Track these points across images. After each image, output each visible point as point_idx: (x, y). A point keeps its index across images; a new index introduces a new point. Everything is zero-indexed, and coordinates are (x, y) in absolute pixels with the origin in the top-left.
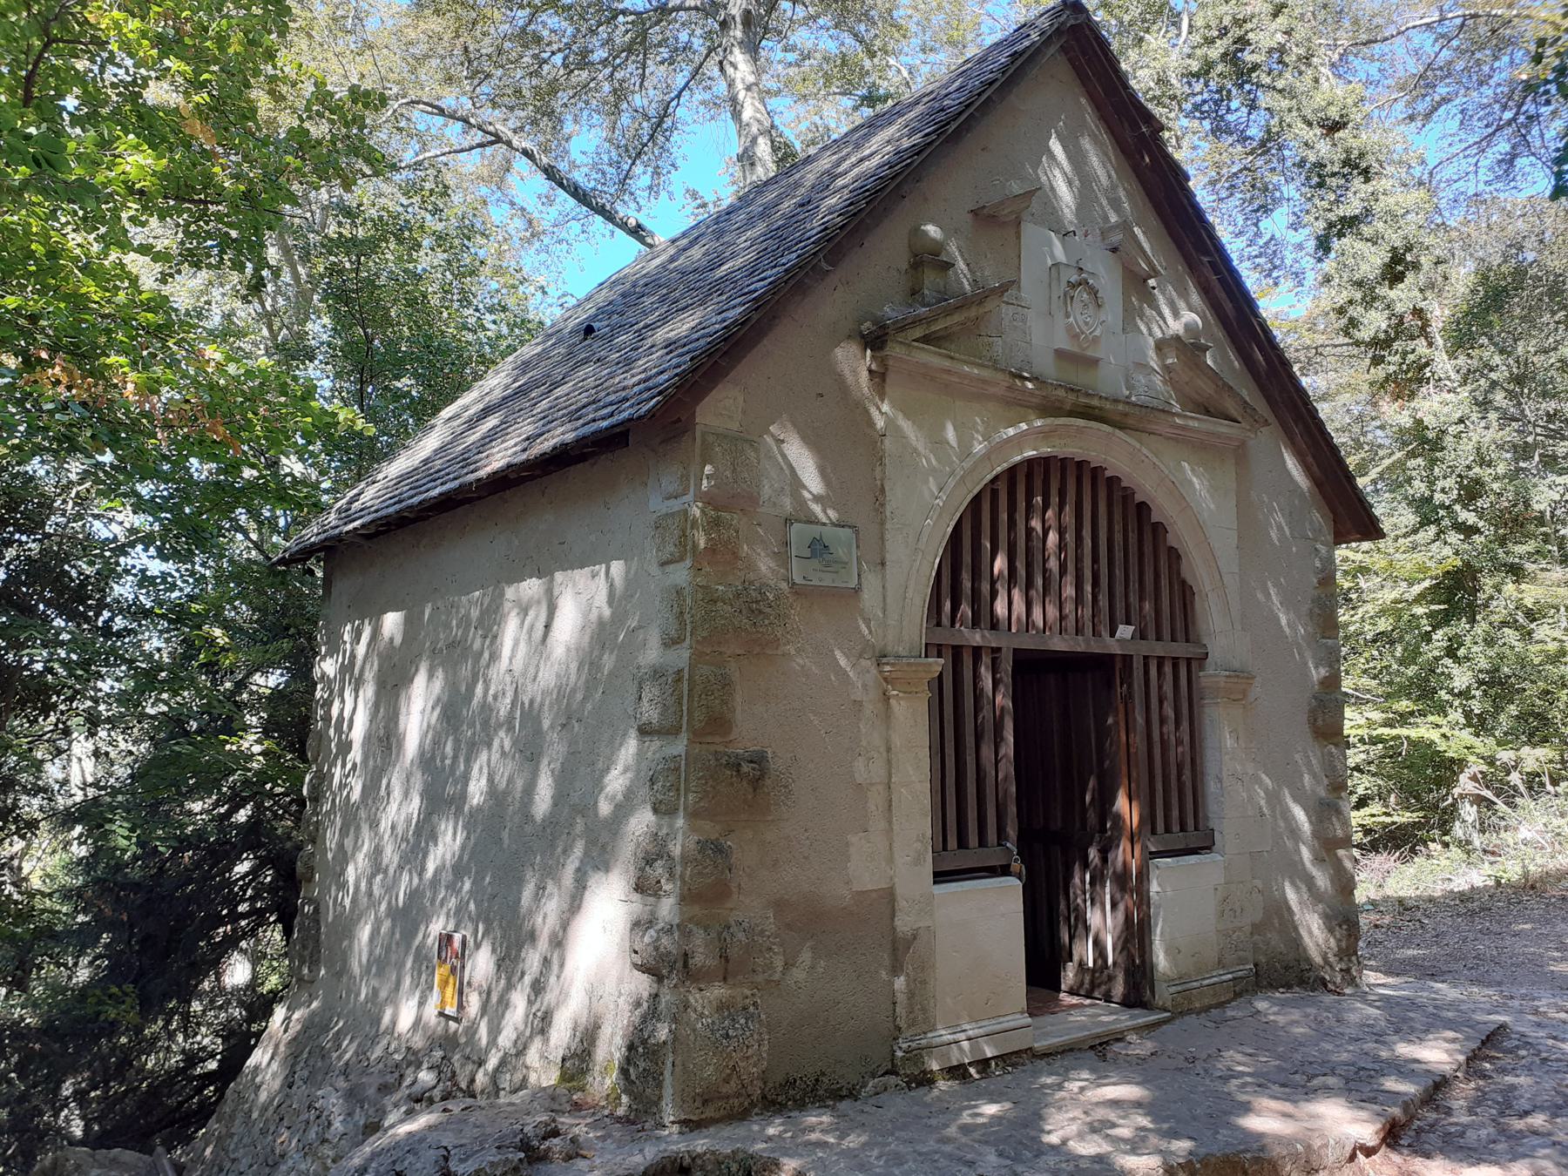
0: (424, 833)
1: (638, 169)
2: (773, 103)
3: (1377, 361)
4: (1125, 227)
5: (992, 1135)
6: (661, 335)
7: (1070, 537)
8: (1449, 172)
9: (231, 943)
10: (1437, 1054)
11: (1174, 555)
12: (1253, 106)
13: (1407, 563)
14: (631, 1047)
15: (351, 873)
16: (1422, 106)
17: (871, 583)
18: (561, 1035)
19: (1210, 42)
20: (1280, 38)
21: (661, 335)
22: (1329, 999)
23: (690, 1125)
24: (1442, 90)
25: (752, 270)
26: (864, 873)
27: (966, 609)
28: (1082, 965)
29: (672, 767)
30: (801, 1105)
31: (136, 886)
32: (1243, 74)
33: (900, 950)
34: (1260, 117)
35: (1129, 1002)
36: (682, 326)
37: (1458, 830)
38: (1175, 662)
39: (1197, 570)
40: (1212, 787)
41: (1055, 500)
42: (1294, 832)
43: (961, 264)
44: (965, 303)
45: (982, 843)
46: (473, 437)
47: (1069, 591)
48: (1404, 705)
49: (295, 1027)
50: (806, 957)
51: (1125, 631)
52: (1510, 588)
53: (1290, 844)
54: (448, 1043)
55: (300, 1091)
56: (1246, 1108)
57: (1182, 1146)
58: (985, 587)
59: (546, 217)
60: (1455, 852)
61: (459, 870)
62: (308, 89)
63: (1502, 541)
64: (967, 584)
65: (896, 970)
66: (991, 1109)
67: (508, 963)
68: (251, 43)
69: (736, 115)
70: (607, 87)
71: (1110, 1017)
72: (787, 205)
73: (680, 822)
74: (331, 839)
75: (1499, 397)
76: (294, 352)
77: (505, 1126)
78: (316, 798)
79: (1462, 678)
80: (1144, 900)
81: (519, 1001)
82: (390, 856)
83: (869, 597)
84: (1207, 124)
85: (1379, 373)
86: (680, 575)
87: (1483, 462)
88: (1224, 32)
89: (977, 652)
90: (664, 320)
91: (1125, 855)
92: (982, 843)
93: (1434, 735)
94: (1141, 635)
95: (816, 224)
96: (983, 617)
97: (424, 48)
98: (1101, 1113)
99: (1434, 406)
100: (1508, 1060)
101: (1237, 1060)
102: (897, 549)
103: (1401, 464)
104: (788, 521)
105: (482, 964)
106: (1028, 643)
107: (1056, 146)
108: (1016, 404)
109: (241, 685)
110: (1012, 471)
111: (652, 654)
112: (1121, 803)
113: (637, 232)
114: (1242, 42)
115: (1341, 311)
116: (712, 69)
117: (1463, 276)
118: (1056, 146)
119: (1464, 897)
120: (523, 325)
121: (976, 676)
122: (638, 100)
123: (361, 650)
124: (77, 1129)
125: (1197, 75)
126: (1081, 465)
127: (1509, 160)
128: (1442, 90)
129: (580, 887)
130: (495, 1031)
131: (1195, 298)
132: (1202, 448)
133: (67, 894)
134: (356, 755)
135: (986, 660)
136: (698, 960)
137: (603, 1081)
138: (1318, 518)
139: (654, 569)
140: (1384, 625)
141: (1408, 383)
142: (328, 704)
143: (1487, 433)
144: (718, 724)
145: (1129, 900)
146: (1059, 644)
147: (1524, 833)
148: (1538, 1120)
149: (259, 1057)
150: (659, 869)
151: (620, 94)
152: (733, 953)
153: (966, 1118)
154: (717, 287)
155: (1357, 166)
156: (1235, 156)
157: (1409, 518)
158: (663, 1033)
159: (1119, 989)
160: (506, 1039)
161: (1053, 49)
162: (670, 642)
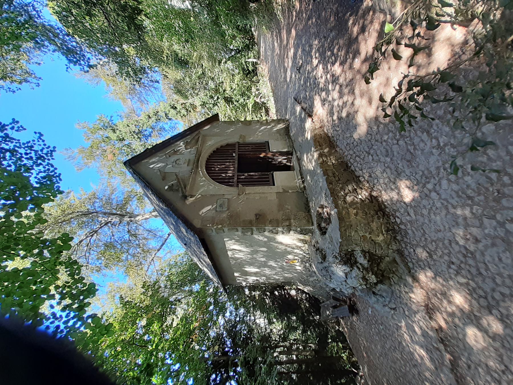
0: (271, 267)
1: (158, 234)
2: (146, 211)
3: (190, 111)
4: (165, 155)
5: (312, 178)
6: (185, 234)
7: (219, 164)
8: (157, 98)
9: (289, 294)
10: (298, 109)
11: (222, 147)
12: (146, 130)
13: (223, 108)
14: (301, 234)
15: (277, 278)
16: (146, 102)
17: (226, 197)
18: (300, 244)
19: (134, 137)
20: (133, 125)
21: (185, 234)
22: (291, 124)
23: (313, 224)
24: (143, 99)
25: (174, 219)
26: (274, 197)
27: (231, 180)
28: (287, 162)
29: (258, 229)
30: (309, 206)
31: (280, 311)
32: (140, 132)
33: (285, 191)
34: (148, 129)
35: (292, 155)
36: (183, 230)
37: (266, 102)
38: (239, 147)
39: (224, 143)
40: (258, 141)
41: (213, 166)
42: (265, 129)
43: (172, 183)
44: (179, 181)
45: (268, 178)
46: (204, 263)
47: (228, 164)
48: (246, 109)
49: (301, 285)
50: (287, 206)
51: (234, 155)
52: (227, 92)
53: (266, 130)
54: (302, 261)
55: (310, 283)
56: (307, 138)
57: (313, 149)
58: (227, 177)
59: (167, 250)
60: (269, 102)
61: (276, 261)
62: (142, 296)
63: (220, 93)
64: (226, 180)
65: (288, 192)
66: (308, 177)
67: (290, 253)
68: (133, 308)
69: (148, 218)
70: (143, 241)
71: (294, 159)
72: (162, 212)
73: (266, 228)
74: (272, 281)
75: (196, 92)
76: (191, 292)
77: (314, 253)
78: (265, 284)
79: (242, 100)
80: (276, 152)
81: (295, 251)
82: (274, 272)
83: (229, 197)
84: (149, 138)
85: (192, 111)
86: (226, 229)
87: (207, 95)
88: (132, 135)
89: (238, 179)
90: (182, 233)
91: (270, 155)
92: (268, 178)
93: (251, 105)
94: (234, 152)
95: (165, 208)
96: (232, 178)
97: (136, 274)
98: (308, 160)
99: (198, 102)
100: (299, 97)
101: (300, 139)
102: (222, 192)
103: (208, 108)
104: (216, 211)
105: (290, 257)
106: (236, 170)
107: (151, 166)
108: (196, 173)
109: (248, 296)
110: (208, 173)
111: (239, 233)
112: (262, 156)
113: (169, 235)
114: (134, 132)
115: (182, 117)
116: (139, 223)
117: (176, 97)
118: (151, 166)
119: (275, 102)
120: (186, 254)
121: (242, 179)
122: (146, 235)
123: (241, 279)
124: (318, 317)
125: (140, 140)
126: (207, 161)
127: (155, 88)
128: (143, 99)
129: (277, 243)
130: (300, 254)
131: (178, 143)
132: (204, 142)
133: (282, 322)
134: (258, 278)
135: (239, 177)
136: (287, 224)
137: (307, 238)
138: (215, 124)
139: (225, 233)
140: (234, 112)
141: (194, 107)
142: (250, 283)
143: (202, 94)
144: (251, 222)
145: (277, 155)
146: (236, 166)
147: (265, 91)
148: (307, 94)
149: (306, 290)
150: (274, 231)
151: (145, 239)
152: (286, 218)
153: (310, 181)
154: (176, 224)
155: (156, 113)
156: (155, 133)
157: (216, 107)
158: (299, 229)
159: (290, 156)
160: (301, 253)
161: (133, 167)
162: (237, 231)
